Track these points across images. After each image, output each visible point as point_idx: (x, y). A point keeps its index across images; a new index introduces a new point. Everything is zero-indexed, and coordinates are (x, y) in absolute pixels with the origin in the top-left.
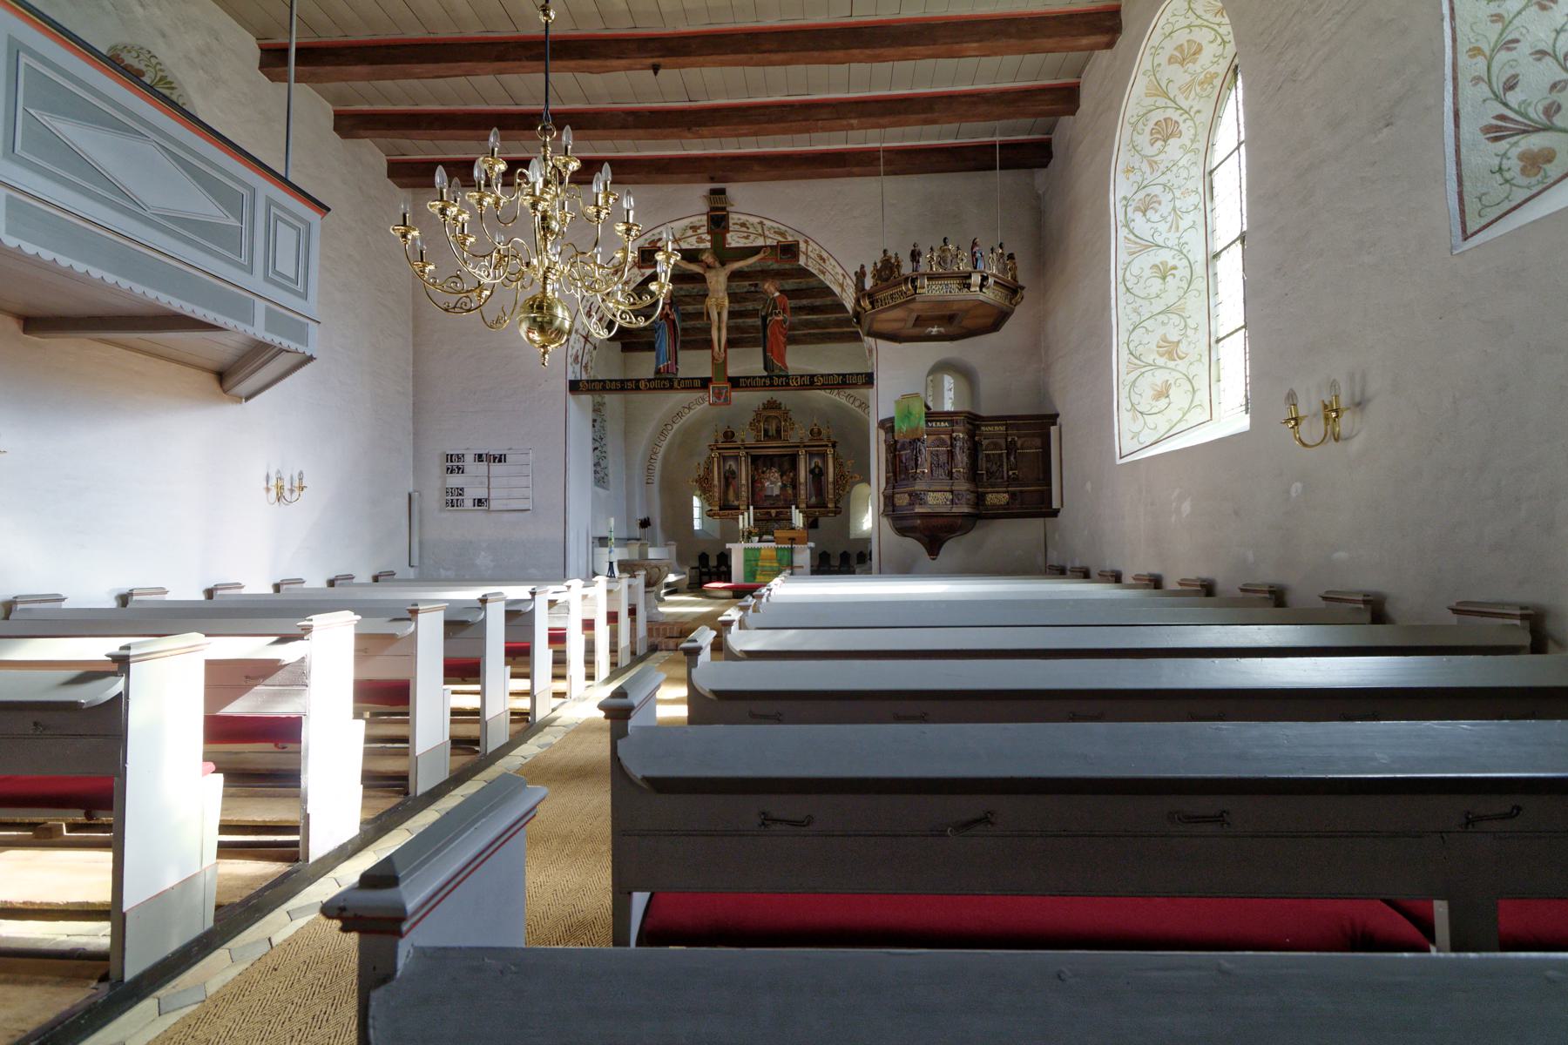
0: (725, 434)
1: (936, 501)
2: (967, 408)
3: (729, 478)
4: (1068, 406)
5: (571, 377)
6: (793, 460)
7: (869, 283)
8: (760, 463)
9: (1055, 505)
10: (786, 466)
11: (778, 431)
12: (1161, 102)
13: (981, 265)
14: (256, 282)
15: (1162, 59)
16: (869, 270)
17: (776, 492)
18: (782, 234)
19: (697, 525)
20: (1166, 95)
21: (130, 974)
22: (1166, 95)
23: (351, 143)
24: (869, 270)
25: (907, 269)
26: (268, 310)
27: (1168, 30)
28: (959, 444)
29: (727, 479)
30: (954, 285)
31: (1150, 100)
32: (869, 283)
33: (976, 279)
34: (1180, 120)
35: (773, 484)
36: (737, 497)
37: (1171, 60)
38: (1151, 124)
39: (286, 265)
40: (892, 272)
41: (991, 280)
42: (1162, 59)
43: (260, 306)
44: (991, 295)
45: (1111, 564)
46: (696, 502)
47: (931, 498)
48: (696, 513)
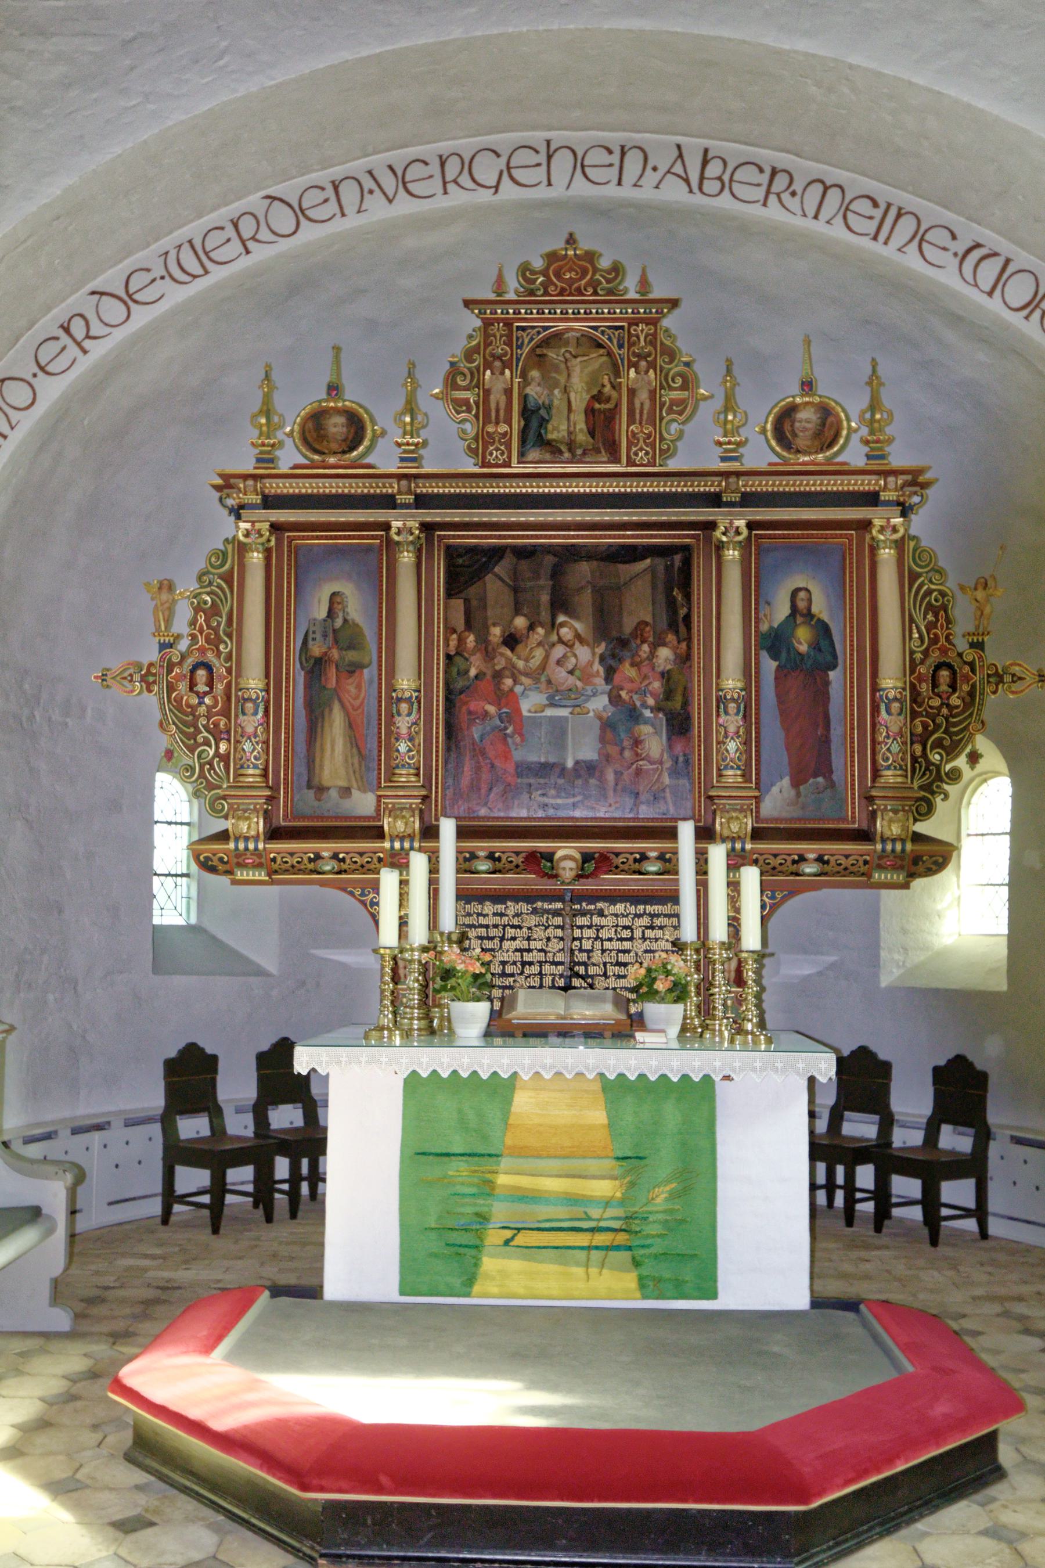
0: (313, 431)
3: (323, 669)
6: (678, 570)
8: (494, 586)
10: (639, 607)
11: (601, 421)
19: (172, 903)
29: (315, 668)
36: (374, 762)
46: (172, 798)
48: (171, 850)
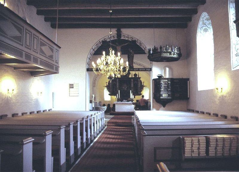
1: (164, 95)
2: (171, 77)
4: (191, 79)
5: (87, 68)
7: (151, 52)
9: (188, 97)
12: (205, 26)
13: (173, 50)
14: (23, 48)
15: (204, 19)
16: (151, 49)
17: (126, 89)
18: (133, 38)
20: (205, 25)
21: (89, 143)
22: (205, 25)
23: (46, 22)
24: (151, 49)
25: (159, 50)
26: (40, 60)
27: (205, 15)
28: (169, 84)
30: (168, 54)
31: (202, 25)
32: (151, 52)
33: (172, 53)
34: (208, 29)
35: (125, 87)
37: (206, 20)
38: (203, 29)
39: (28, 44)
40: (156, 51)
41: (175, 53)
42: (204, 19)
43: (55, 66)
44: (175, 56)
45: (197, 110)
47: (164, 95)
